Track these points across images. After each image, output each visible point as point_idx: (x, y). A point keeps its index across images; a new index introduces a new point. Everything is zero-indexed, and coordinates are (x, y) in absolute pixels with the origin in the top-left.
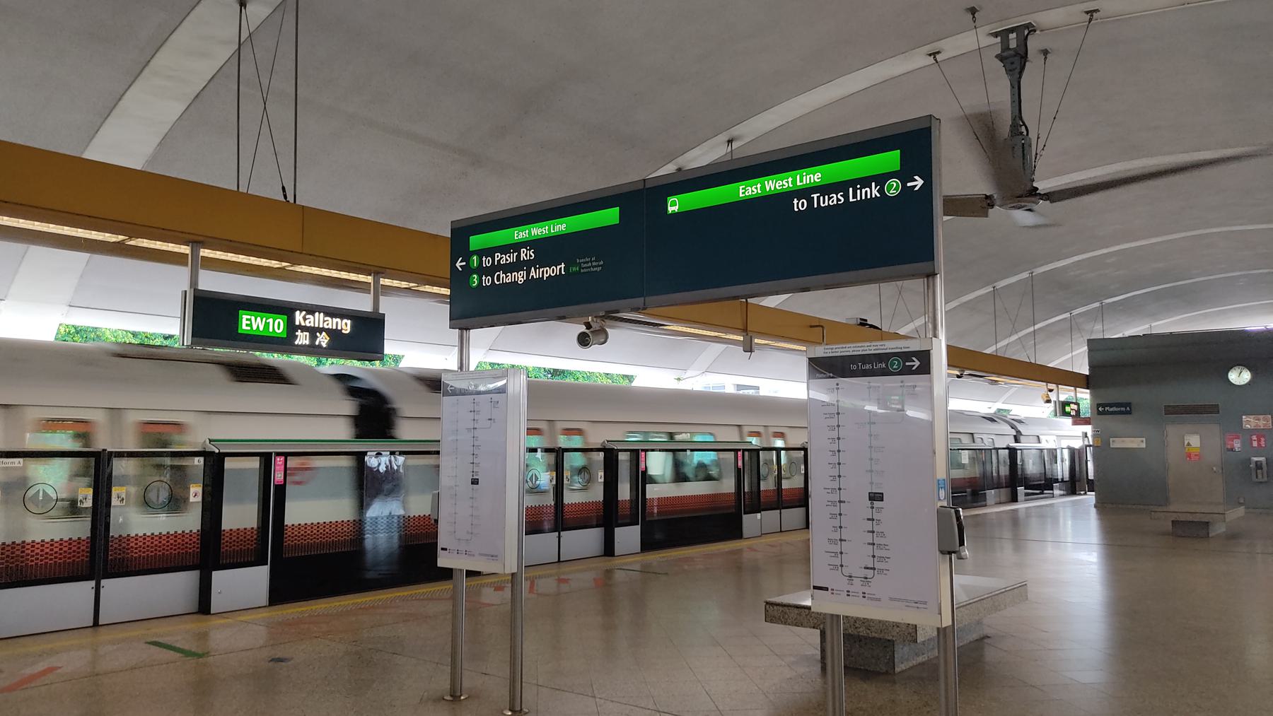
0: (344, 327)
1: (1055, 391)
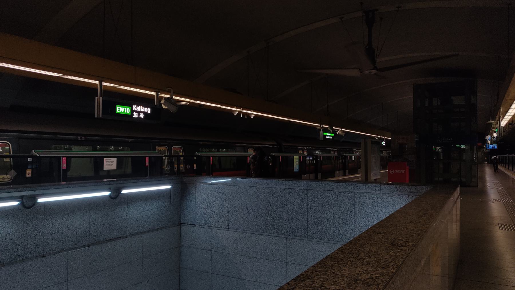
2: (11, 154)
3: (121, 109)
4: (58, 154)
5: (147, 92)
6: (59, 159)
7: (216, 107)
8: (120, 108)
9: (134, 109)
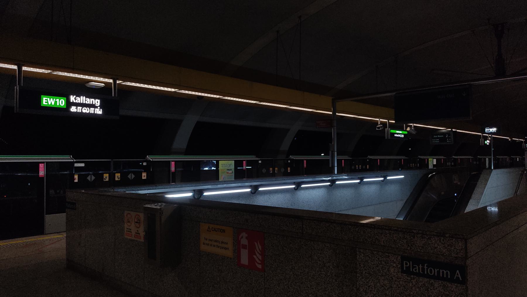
0: (96, 103)
2: (487, 159)
3: (48, 101)
4: (168, 158)
5: (212, 96)
6: (169, 163)
7: (312, 111)
8: (49, 99)
9: (72, 101)
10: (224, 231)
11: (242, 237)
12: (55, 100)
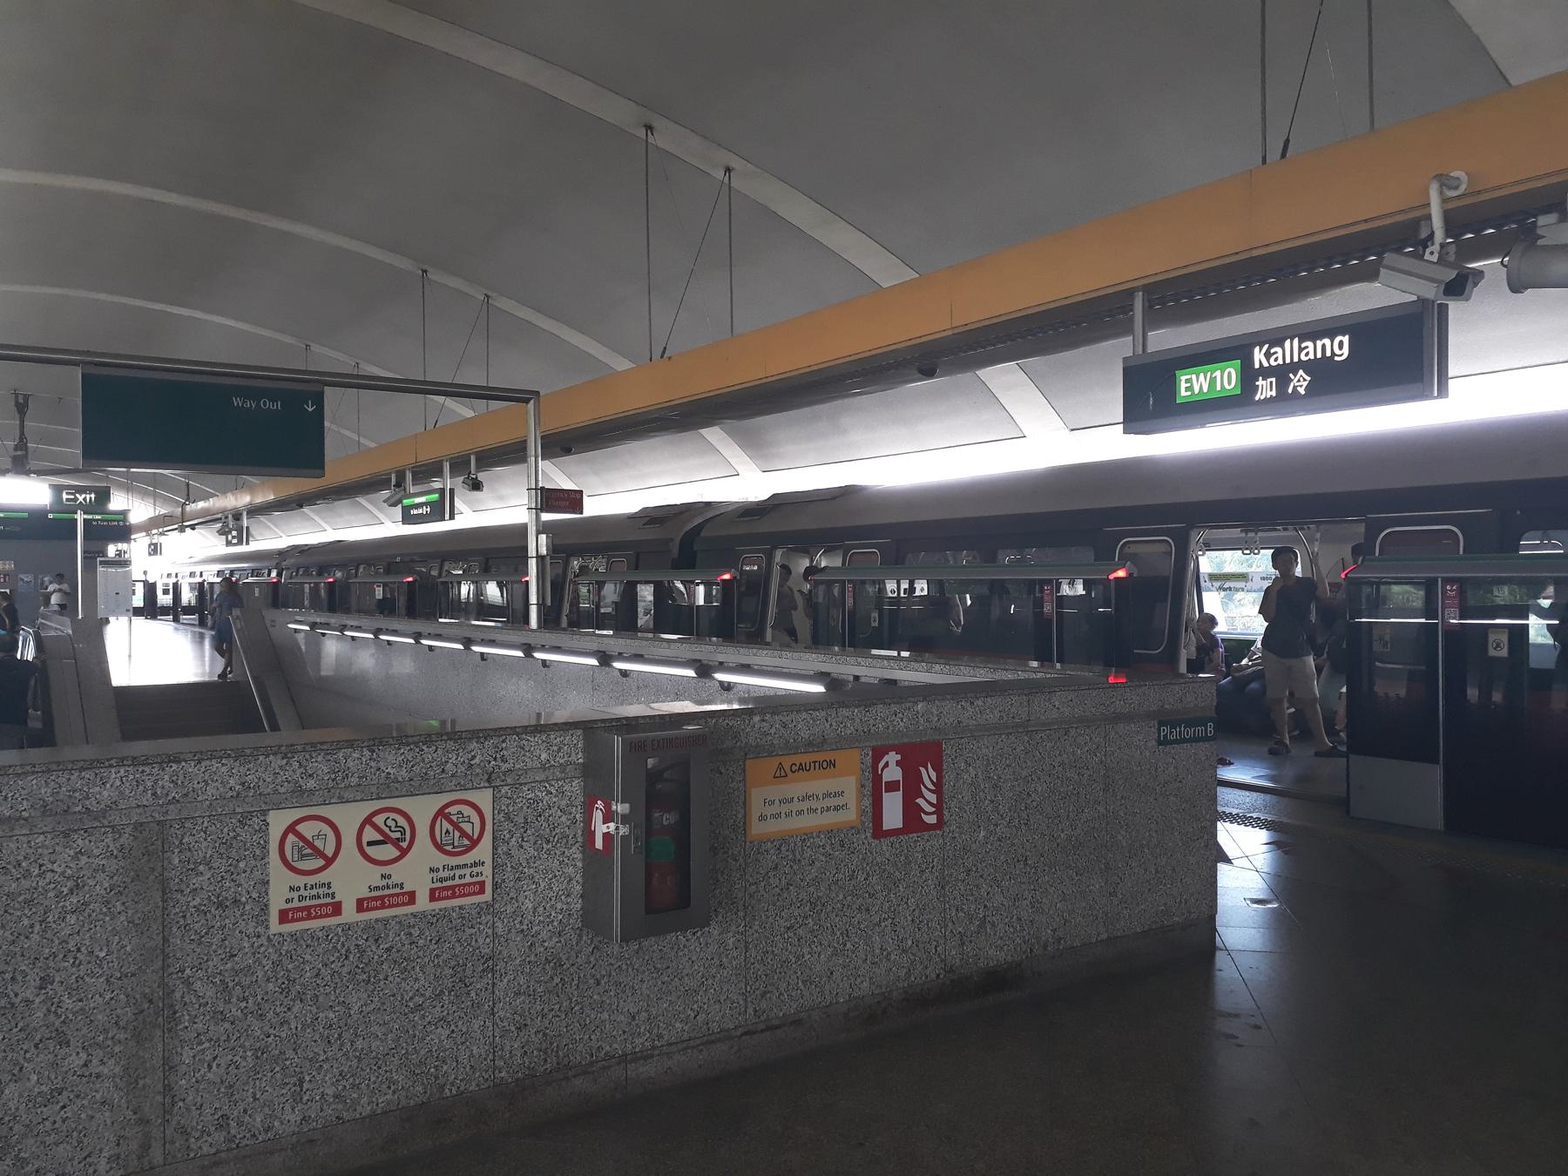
0: (1337, 351)
1: (704, 1050)
10: (832, 764)
11: (887, 765)
12: (1211, 375)
